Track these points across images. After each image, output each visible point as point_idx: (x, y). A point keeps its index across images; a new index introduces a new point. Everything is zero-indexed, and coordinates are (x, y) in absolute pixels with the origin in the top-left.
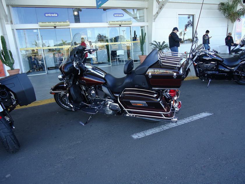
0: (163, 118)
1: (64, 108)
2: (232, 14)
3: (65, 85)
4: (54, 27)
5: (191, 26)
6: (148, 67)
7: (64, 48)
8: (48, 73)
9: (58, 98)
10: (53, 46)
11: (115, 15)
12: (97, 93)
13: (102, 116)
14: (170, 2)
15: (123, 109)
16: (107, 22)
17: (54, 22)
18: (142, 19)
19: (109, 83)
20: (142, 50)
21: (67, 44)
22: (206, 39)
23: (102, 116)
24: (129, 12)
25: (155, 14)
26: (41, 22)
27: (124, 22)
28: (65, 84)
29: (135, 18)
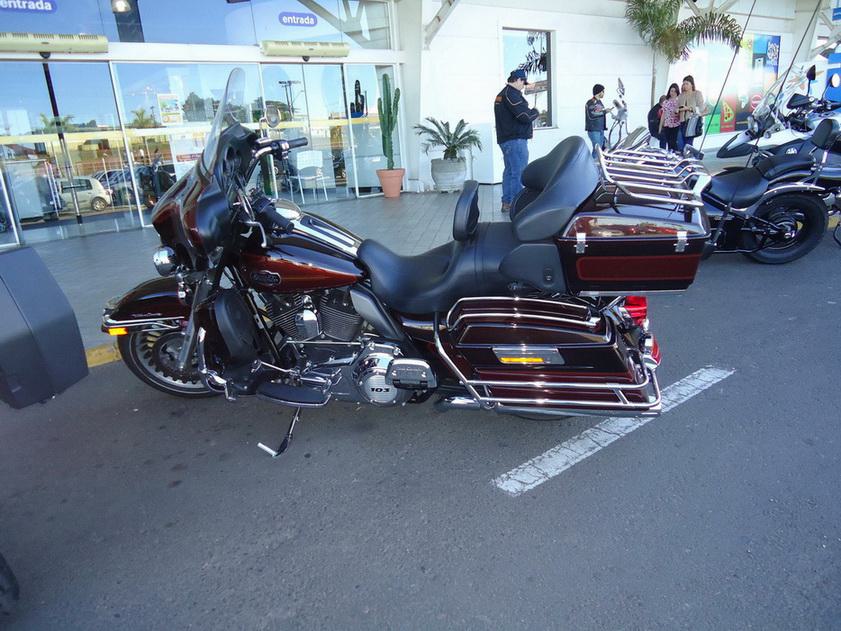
0: (621, 404)
1: (164, 390)
2: (668, 32)
3: (182, 295)
4: (42, 53)
5: (538, 70)
6: (574, 209)
7: (335, 123)
9: (138, 350)
10: (27, 134)
11: (285, 19)
12: (322, 320)
13: (353, 411)
15: (458, 379)
16: (257, 45)
17: (41, 36)
18: (380, 38)
19: (382, 278)
20: (387, 150)
21: (77, 129)
22: (597, 113)
23: (353, 411)
24: (325, 10)
25: (428, 23)
27: (318, 47)
28: (184, 290)
29: (355, 34)
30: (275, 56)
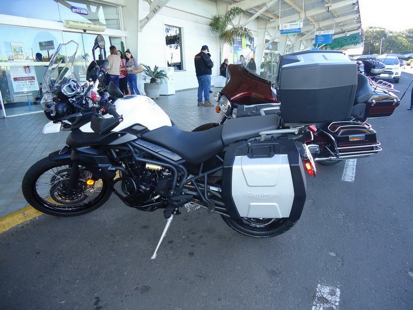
14: (168, 7)
30: (71, 28)
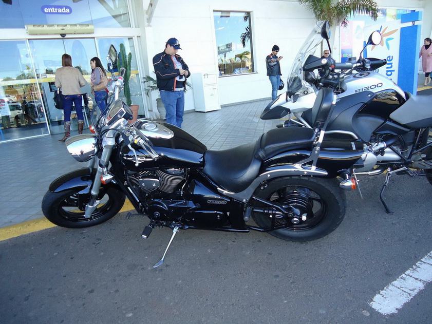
8: (52, 134)
26: (31, 24)
